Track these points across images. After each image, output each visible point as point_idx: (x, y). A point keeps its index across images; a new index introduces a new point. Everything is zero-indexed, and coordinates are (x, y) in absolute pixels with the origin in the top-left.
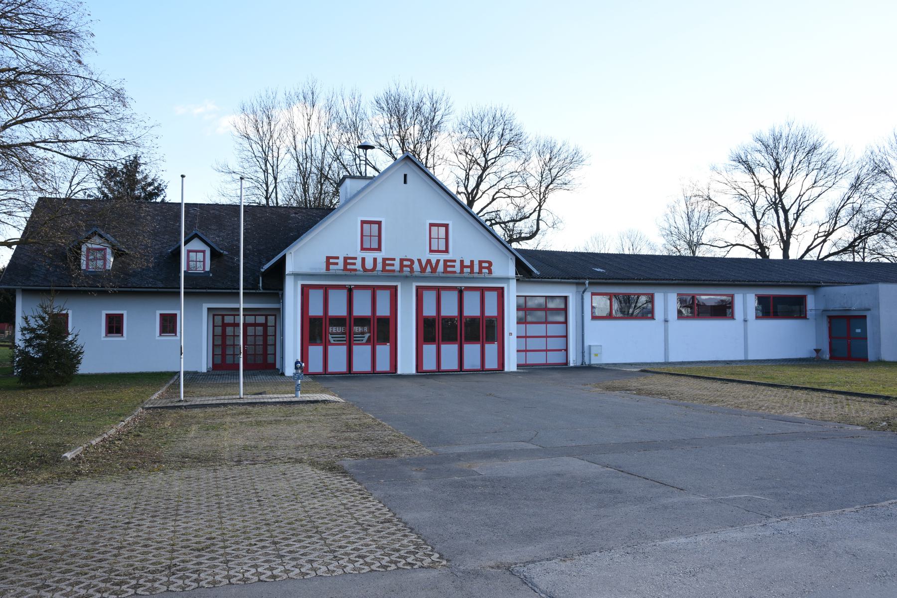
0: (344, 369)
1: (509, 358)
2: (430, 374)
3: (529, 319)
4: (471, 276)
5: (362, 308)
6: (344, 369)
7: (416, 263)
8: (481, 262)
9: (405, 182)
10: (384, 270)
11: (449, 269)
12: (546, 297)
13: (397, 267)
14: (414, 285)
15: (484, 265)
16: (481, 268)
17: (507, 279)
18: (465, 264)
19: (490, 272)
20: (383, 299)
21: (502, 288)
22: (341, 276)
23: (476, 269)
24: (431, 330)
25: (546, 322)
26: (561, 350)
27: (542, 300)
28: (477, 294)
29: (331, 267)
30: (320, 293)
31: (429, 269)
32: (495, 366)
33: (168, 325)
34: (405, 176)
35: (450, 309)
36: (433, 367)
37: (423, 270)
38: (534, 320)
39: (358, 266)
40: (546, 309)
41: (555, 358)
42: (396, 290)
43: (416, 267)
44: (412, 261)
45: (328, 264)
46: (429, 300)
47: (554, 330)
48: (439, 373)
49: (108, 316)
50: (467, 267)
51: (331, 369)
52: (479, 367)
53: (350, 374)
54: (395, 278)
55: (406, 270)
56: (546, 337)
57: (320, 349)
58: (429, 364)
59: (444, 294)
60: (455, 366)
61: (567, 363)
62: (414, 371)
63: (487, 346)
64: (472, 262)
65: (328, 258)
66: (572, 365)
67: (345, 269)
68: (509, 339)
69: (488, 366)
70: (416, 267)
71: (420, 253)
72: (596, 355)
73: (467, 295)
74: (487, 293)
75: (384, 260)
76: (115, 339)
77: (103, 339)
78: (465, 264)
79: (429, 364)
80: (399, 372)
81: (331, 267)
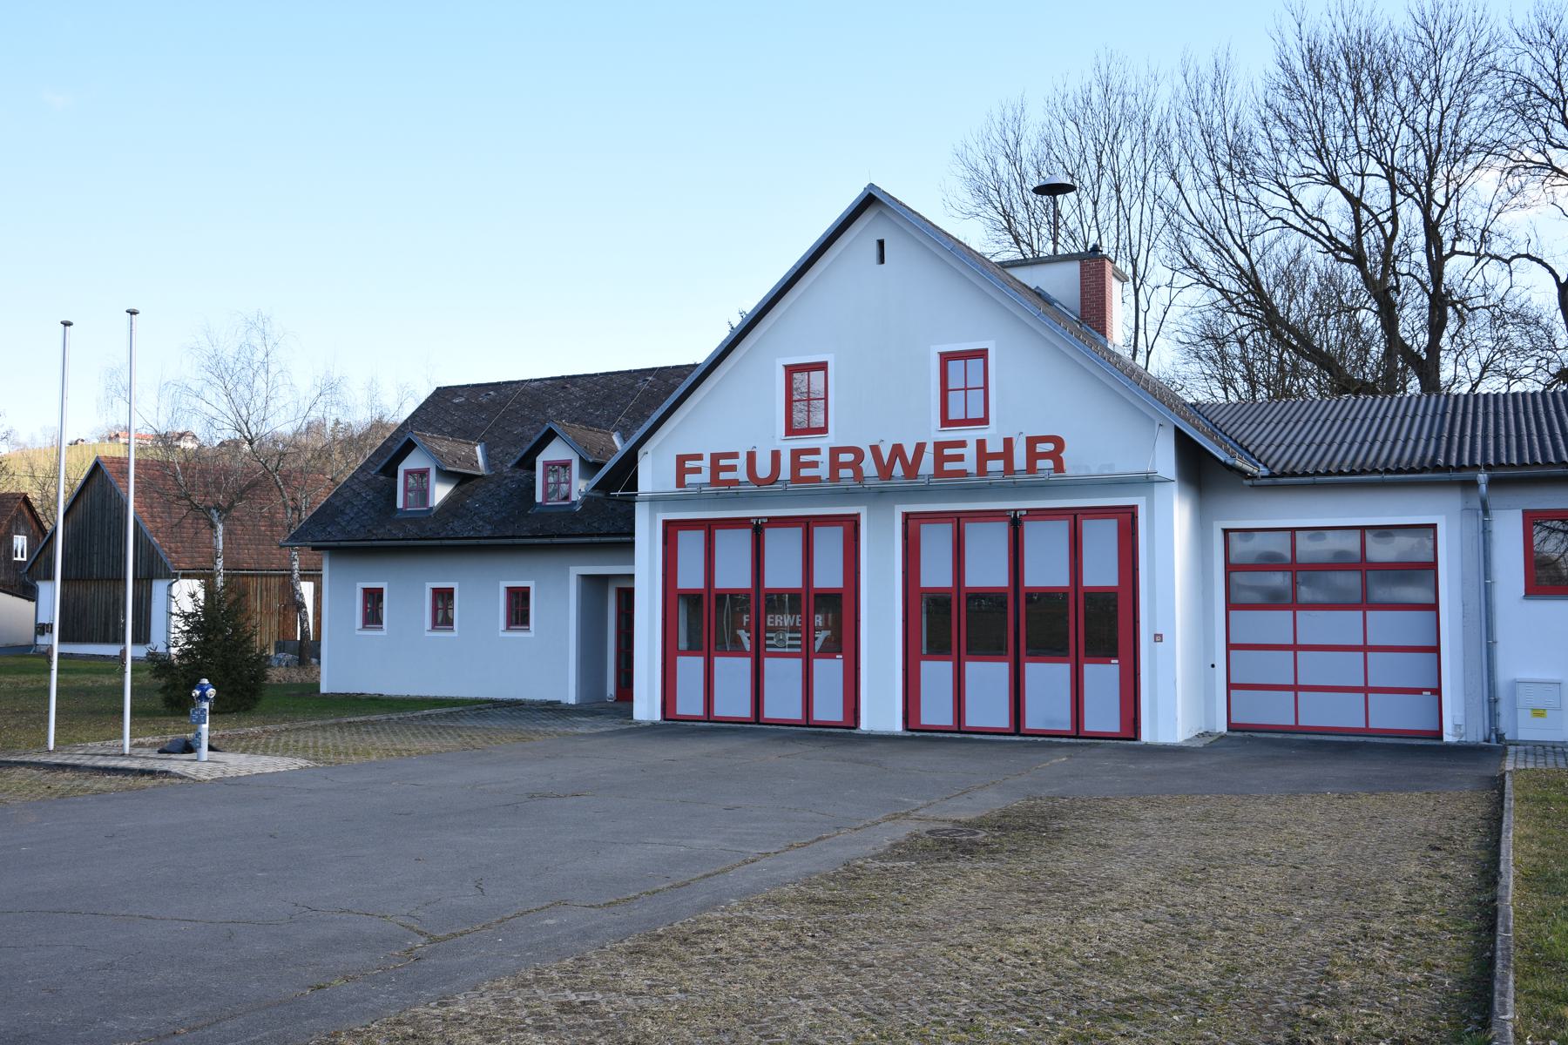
0: (796, 714)
1: (1154, 704)
2: (732, 726)
3: (1305, 594)
4: (1009, 479)
5: (783, 573)
6: (745, 711)
7: (868, 455)
8: (1032, 442)
9: (882, 260)
10: (796, 477)
11: (804, 472)
12: (1363, 528)
13: (823, 471)
14: (900, 510)
15: (1042, 448)
16: (1032, 456)
17: (1147, 482)
18: (990, 449)
19: (1059, 467)
20: (829, 544)
21: (1132, 511)
22: (730, 501)
23: (1020, 461)
24: (949, 624)
25: (1365, 604)
26: (1418, 691)
27: (1351, 543)
28: (796, 534)
29: (689, 478)
30: (699, 536)
31: (898, 470)
32: (1114, 726)
33: (518, 609)
34: (881, 243)
35: (987, 569)
36: (947, 719)
37: (885, 471)
38: (1321, 597)
39: (741, 474)
40: (1363, 565)
41: (1391, 714)
42: (1134, 518)
43: (869, 467)
44: (858, 452)
45: (681, 472)
46: (937, 544)
47: (1386, 627)
48: (710, 725)
49: (436, 591)
50: (995, 456)
51: (719, 711)
52: (1067, 727)
53: (756, 723)
54: (848, 495)
55: (895, 472)
56: (1295, 647)
57: (1062, 671)
58: (936, 712)
59: (972, 530)
60: (1000, 718)
61: (1439, 734)
62: (897, 727)
63: (1090, 670)
64: (1008, 443)
65: (681, 459)
66: (1449, 737)
67: (715, 480)
68: (1152, 653)
69: (819, 715)
70: (869, 467)
71: (917, 425)
72: (1538, 713)
73: (1033, 533)
74: (771, 535)
75: (835, 452)
76: (1541, 720)
77: (502, 634)
78: (990, 449)
79: (936, 712)
80: (865, 725)
81: (689, 478)
